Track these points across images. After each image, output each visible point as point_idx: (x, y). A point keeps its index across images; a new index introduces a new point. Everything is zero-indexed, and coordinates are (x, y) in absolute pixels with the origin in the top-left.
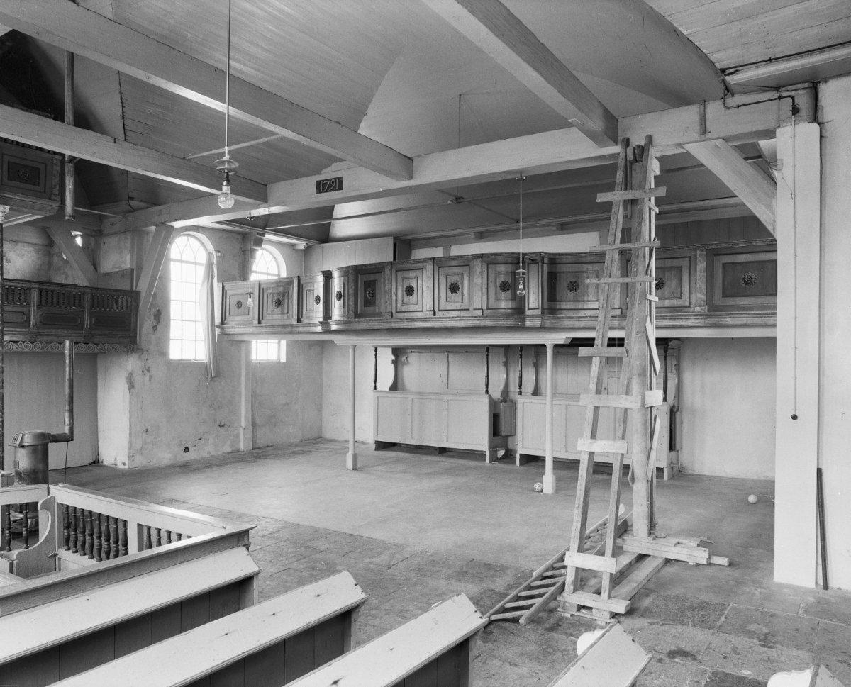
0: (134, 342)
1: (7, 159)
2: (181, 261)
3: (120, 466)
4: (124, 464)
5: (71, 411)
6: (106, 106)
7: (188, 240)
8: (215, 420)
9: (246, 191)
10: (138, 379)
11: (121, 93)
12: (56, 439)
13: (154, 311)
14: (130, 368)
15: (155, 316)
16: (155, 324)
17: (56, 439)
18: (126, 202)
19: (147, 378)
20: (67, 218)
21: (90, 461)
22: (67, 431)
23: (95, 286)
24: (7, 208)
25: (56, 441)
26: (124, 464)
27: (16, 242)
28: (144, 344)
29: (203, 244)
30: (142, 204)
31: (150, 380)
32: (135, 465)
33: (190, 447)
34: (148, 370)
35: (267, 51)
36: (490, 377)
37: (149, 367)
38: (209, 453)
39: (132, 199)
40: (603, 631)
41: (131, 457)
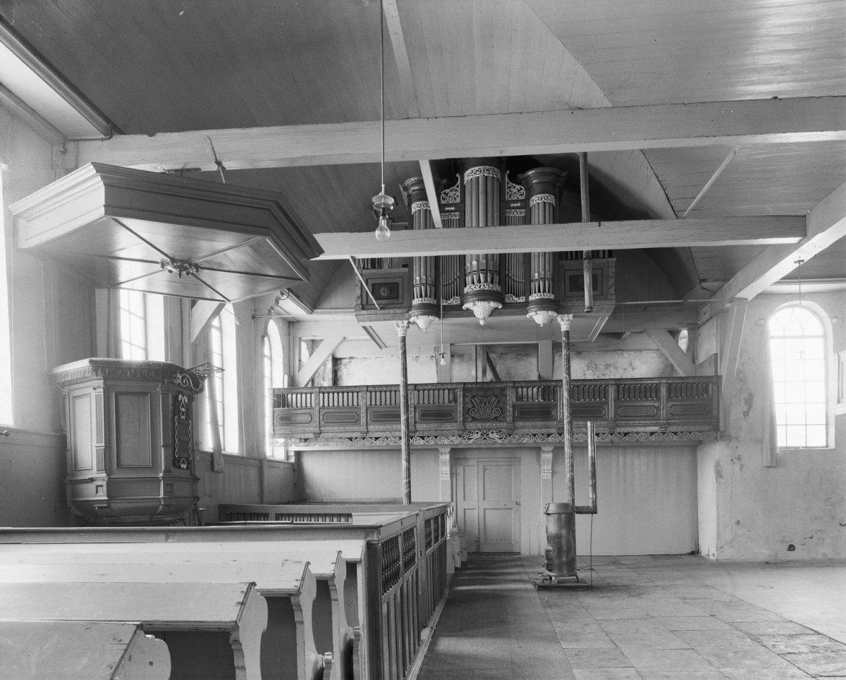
0: (716, 429)
1: (568, 274)
2: (784, 337)
3: (712, 558)
4: (714, 555)
5: (594, 486)
6: (652, 194)
7: (793, 312)
8: (833, 518)
9: (477, 244)
10: (727, 468)
11: (657, 177)
12: (582, 511)
13: (744, 395)
14: (717, 457)
15: (746, 400)
16: (746, 409)
17: (582, 511)
18: (699, 286)
19: (737, 467)
20: (586, 310)
21: (689, 551)
22: (591, 505)
23: (694, 375)
24: (571, 316)
25: (581, 513)
26: (714, 555)
27: (640, 350)
28: (733, 432)
29: (815, 313)
30: (717, 284)
31: (741, 469)
32: (725, 557)
33: (796, 545)
34: (739, 458)
35: (796, 51)
36: (149, 319)
37: (739, 456)
38: (825, 555)
39: (704, 280)
40: (450, 570)
41: (720, 548)
